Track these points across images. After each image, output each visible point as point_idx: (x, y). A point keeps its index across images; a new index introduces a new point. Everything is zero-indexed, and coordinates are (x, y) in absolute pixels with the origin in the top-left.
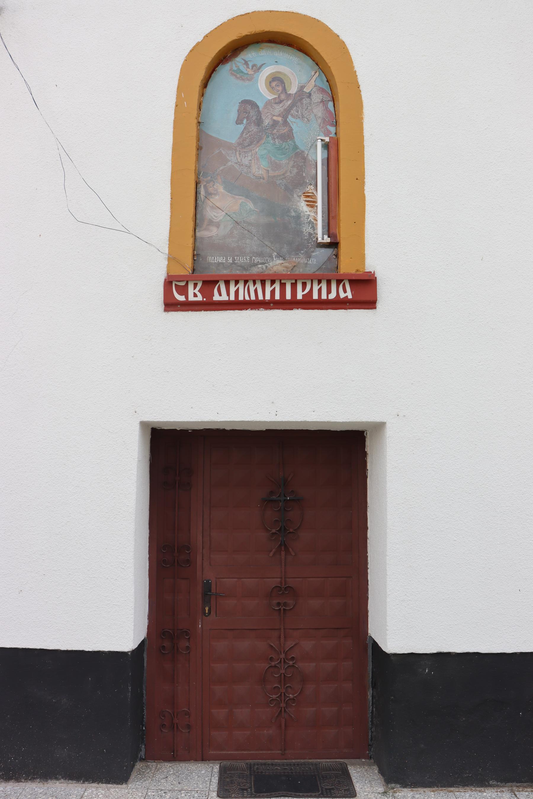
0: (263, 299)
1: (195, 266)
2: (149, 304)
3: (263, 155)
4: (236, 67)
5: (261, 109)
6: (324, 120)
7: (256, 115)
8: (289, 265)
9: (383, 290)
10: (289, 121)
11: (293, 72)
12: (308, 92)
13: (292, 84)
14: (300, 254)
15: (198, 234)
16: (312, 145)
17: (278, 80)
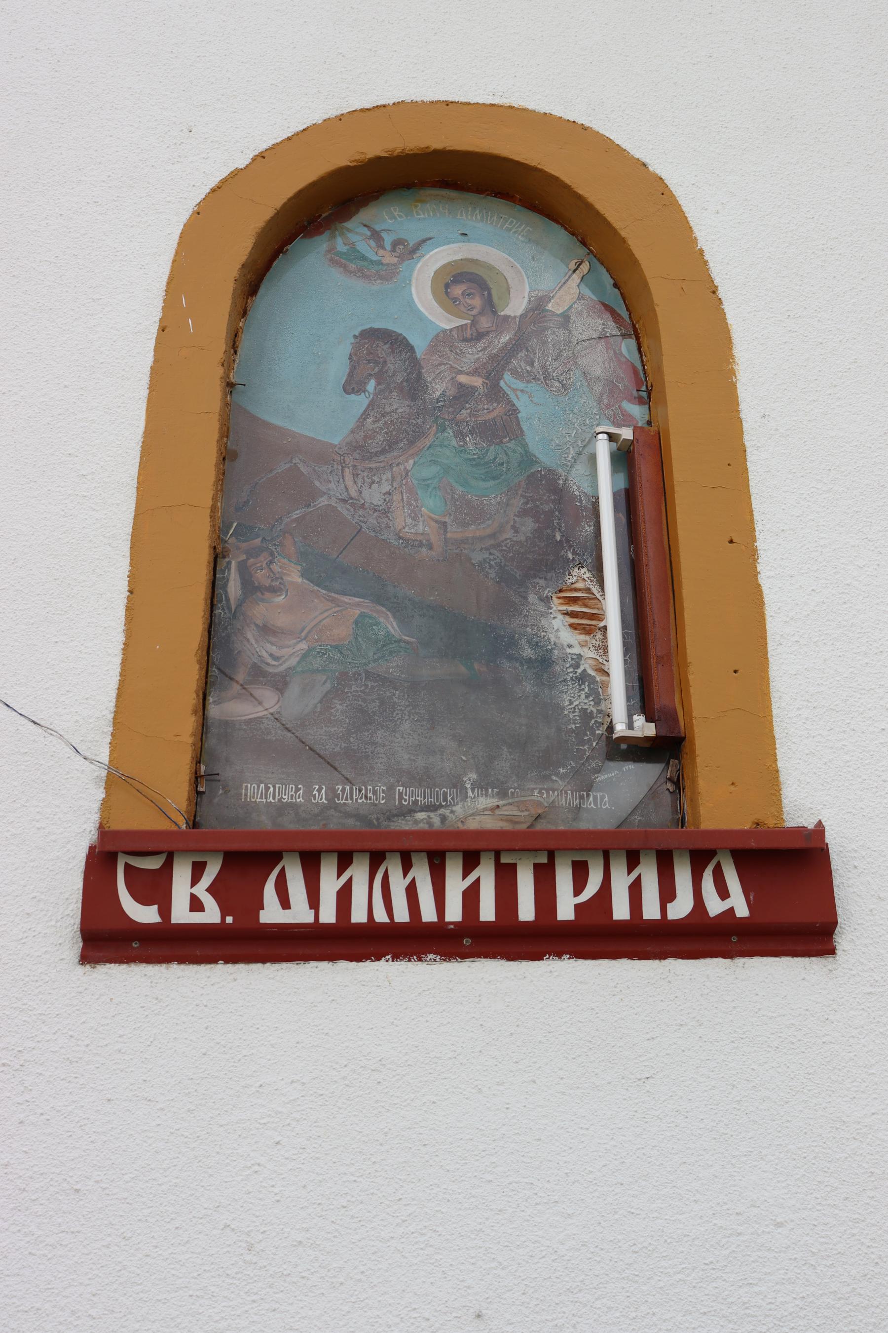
0: (436, 920)
1: (198, 814)
2: (26, 935)
3: (428, 480)
4: (345, 245)
5: (419, 352)
6: (611, 387)
7: (406, 370)
8: (519, 814)
9: (851, 890)
10: (504, 388)
11: (512, 260)
12: (559, 312)
13: (512, 291)
14: (554, 778)
15: (214, 711)
16: (579, 454)
17: (470, 281)
